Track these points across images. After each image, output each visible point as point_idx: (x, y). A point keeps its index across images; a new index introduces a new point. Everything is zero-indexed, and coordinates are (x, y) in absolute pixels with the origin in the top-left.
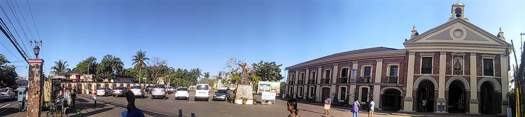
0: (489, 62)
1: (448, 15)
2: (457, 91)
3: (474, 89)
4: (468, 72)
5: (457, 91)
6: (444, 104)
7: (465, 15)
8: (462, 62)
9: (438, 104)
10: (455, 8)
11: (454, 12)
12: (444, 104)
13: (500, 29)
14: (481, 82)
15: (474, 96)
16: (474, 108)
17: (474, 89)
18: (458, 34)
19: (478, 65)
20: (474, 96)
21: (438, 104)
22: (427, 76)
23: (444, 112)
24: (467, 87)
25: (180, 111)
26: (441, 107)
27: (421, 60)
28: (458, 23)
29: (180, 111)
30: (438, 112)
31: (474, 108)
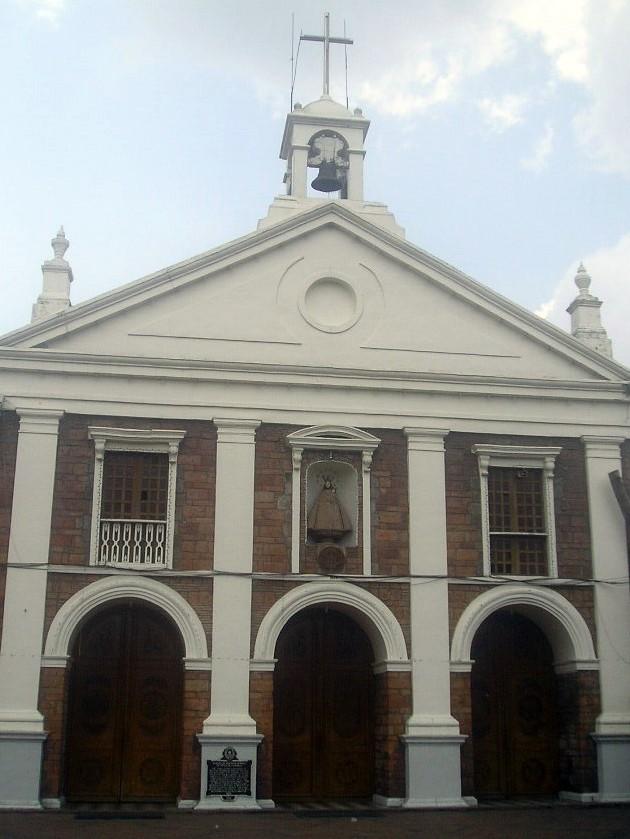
0: (516, 491)
1: (254, 191)
2: (330, 679)
3: (429, 652)
4: (394, 552)
5: (330, 679)
6: (247, 754)
7: (377, 182)
8: (362, 496)
9: (210, 754)
10: (302, 136)
11: (301, 157)
12: (247, 754)
13: (583, 282)
14: (478, 609)
15: (432, 715)
16: (434, 781)
17: (429, 652)
18: (332, 312)
19: (459, 511)
20: (432, 715)
21: (210, 754)
22: (125, 578)
23: (246, 803)
24: (394, 653)
25: (352, 43)
26: (229, 776)
27: (99, 469)
28: (331, 240)
29: (352, 43)
30: (207, 803)
31: (434, 781)
